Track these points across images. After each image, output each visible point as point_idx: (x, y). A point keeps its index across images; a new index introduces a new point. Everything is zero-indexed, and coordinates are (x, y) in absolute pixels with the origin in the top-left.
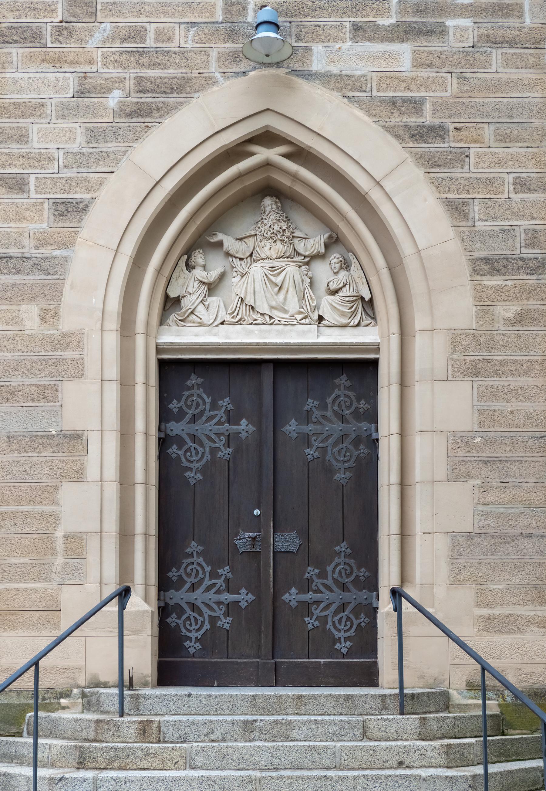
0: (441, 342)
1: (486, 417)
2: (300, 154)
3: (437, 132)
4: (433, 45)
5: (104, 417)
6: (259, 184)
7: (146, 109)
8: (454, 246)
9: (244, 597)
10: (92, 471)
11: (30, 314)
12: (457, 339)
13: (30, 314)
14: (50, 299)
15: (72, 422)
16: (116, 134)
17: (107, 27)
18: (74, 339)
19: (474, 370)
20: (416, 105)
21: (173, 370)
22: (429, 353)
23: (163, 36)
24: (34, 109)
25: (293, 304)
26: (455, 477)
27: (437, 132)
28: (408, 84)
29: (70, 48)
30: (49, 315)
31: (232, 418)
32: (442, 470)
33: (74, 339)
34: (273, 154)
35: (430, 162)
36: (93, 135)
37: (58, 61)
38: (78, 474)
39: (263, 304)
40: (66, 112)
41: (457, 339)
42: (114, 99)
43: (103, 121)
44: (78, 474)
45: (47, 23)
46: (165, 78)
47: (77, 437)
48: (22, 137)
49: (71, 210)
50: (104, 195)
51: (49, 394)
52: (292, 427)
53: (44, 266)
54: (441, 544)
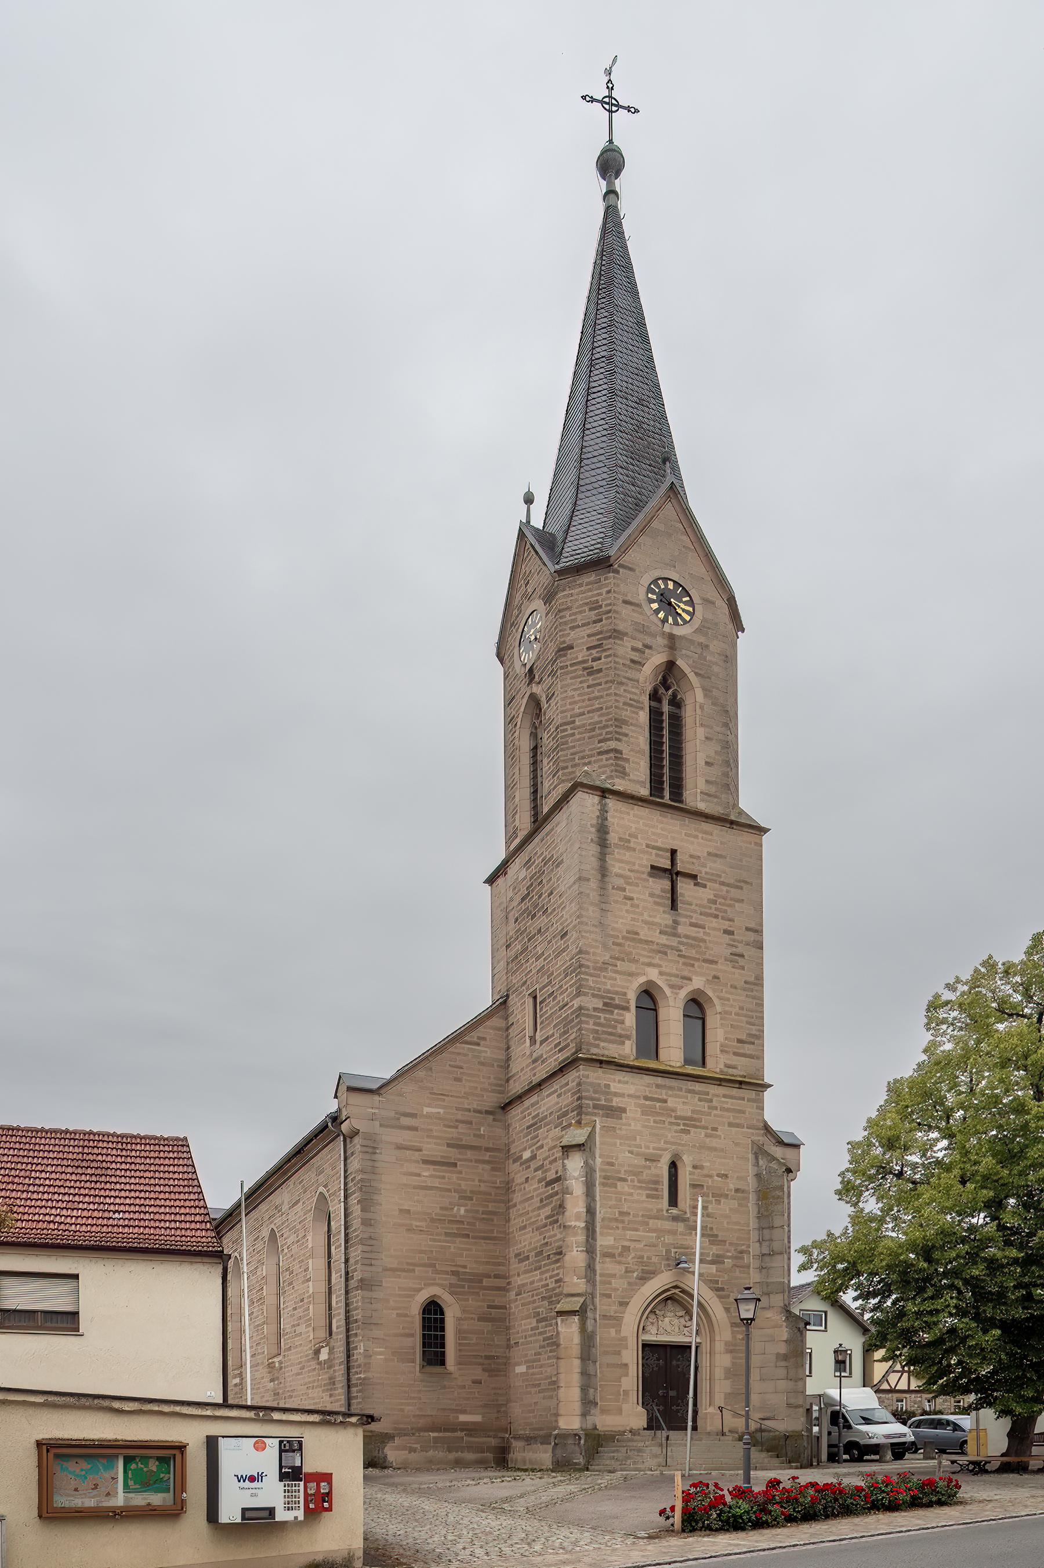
0: (723, 1344)
1: (734, 1364)
2: (683, 1291)
3: (722, 1289)
4: (722, 1266)
5: (631, 1357)
6: (675, 1299)
7: (646, 1277)
8: (726, 1320)
9: (674, 1408)
10: (630, 1374)
11: (613, 1331)
12: (727, 1343)
13: (613, 1331)
14: (618, 1326)
15: (624, 1361)
16: (636, 1284)
17: (633, 1255)
18: (625, 1339)
19: (731, 1352)
20: (717, 1282)
21: (647, 1347)
22: (719, 1346)
23: (649, 1258)
24: (614, 1276)
25: (677, 1330)
26: (726, 1378)
27: (722, 1289)
28: (715, 1276)
29: (623, 1259)
30: (618, 1332)
31: (658, 1360)
32: (723, 1377)
33: (625, 1339)
34: (677, 1291)
35: (720, 1297)
36: (629, 1283)
37: (620, 1263)
38: (627, 1375)
39: (670, 1330)
40: (621, 1277)
41: (727, 1343)
42: (635, 1275)
43: (632, 1280)
44: (627, 1375)
45: (617, 1252)
46: (241, 1375)
47: (626, 1365)
48: (610, 1283)
49: (624, 1304)
50: (633, 1300)
51: (619, 1353)
52: (674, 1363)
53: (615, 1318)
54: (722, 1396)
